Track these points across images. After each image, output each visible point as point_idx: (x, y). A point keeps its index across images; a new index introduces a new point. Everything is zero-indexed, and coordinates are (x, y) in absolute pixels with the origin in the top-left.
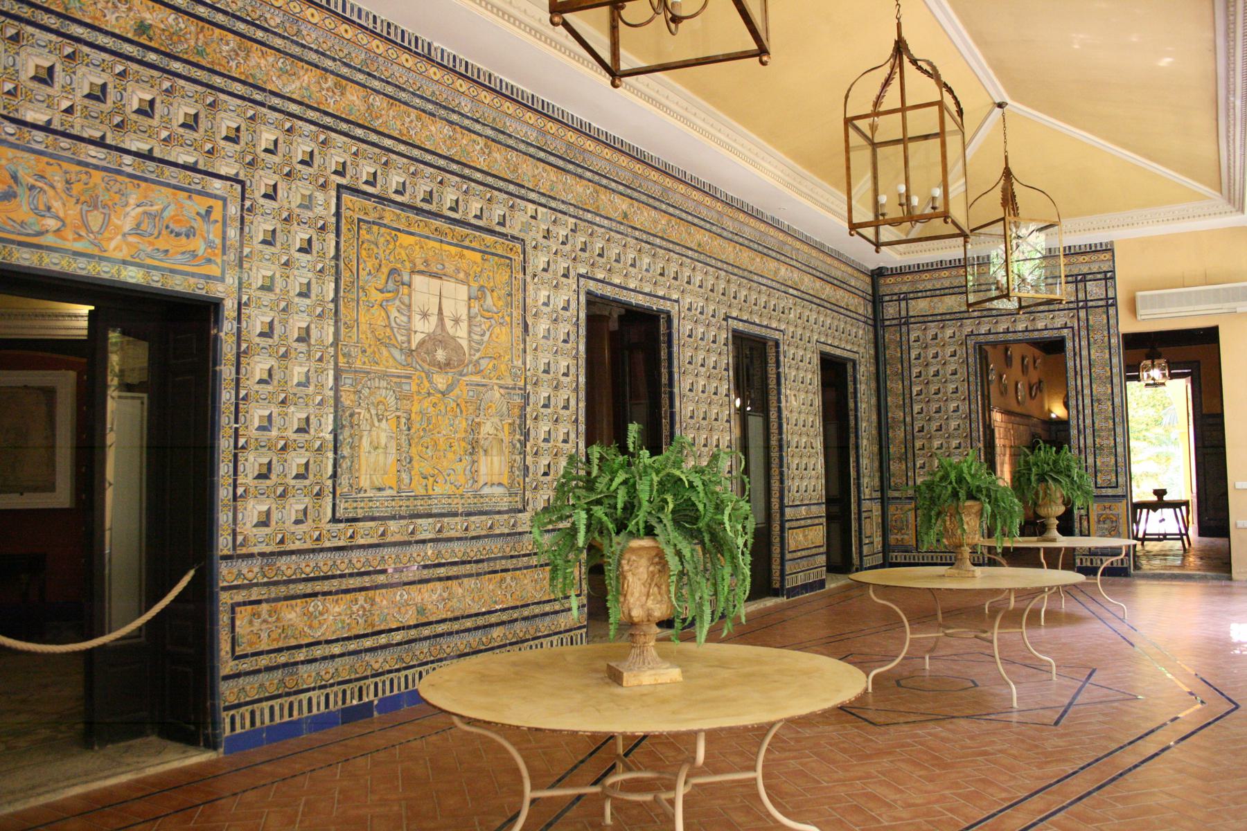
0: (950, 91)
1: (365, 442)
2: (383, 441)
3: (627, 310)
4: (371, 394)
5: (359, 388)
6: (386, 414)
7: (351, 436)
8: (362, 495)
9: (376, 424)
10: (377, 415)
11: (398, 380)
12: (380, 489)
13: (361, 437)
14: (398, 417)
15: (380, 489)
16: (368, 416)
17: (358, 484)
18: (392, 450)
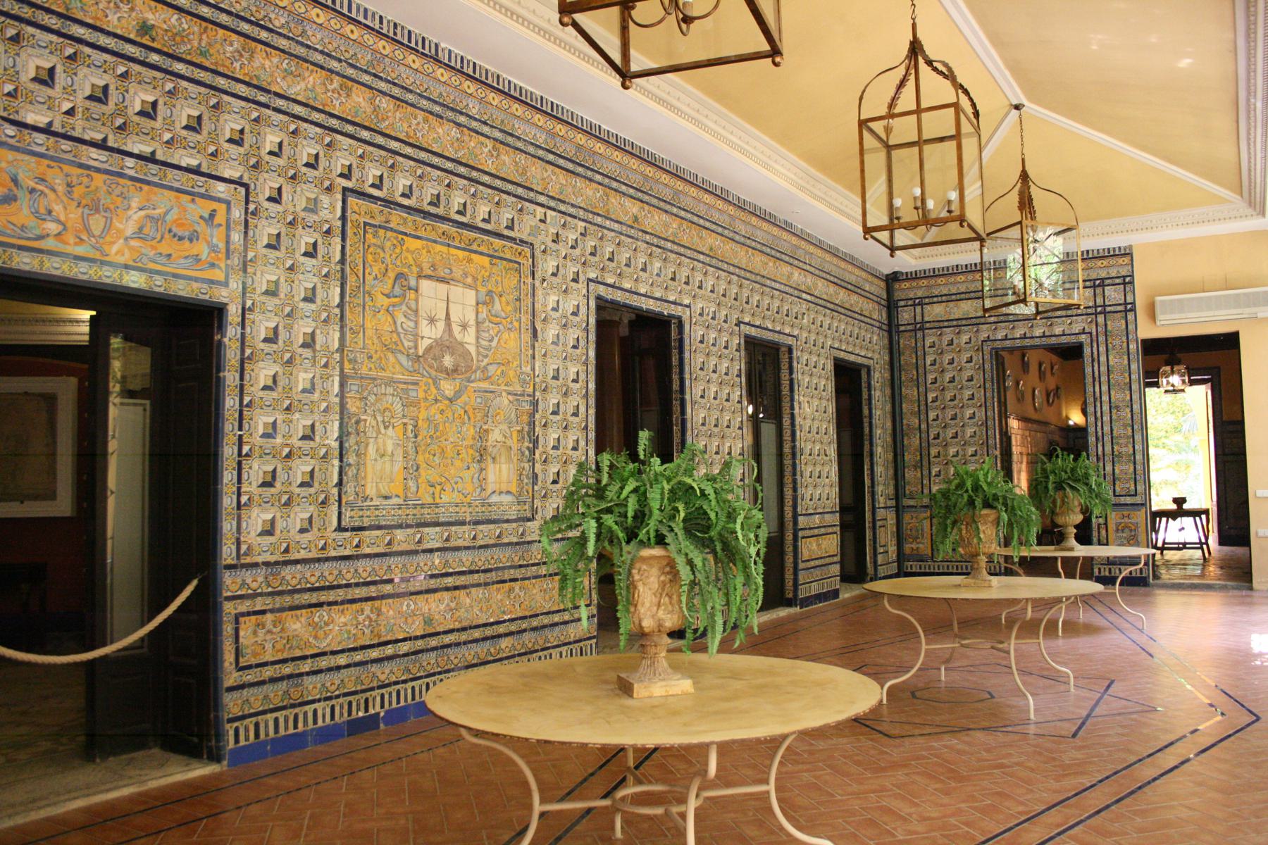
0: (966, 92)
1: (371, 450)
2: (390, 448)
3: (637, 316)
4: (377, 401)
5: (365, 394)
6: (393, 421)
7: (357, 443)
8: (368, 503)
9: (383, 431)
10: (384, 422)
11: (405, 386)
12: (386, 498)
13: (367, 445)
14: (405, 424)
15: (386, 498)
16: (374, 423)
17: (364, 492)
18: (399, 457)
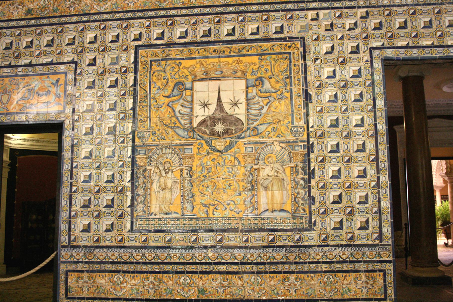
1: (155, 186)
4: (159, 158)
5: (150, 155)
6: (171, 168)
7: (144, 183)
8: (153, 216)
9: (164, 174)
10: (164, 170)
12: (166, 214)
13: (152, 183)
14: (182, 170)
15: (166, 214)
16: (157, 171)
17: (150, 210)
18: (177, 188)
